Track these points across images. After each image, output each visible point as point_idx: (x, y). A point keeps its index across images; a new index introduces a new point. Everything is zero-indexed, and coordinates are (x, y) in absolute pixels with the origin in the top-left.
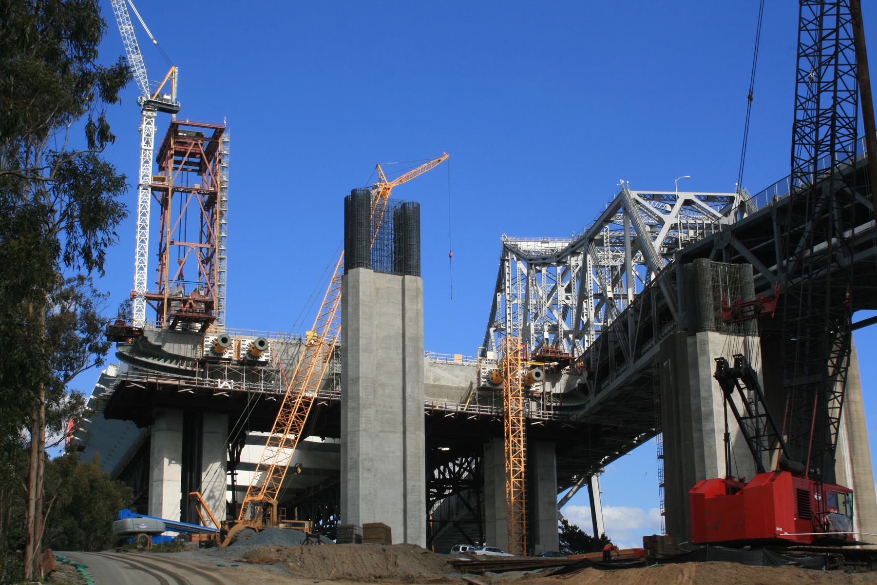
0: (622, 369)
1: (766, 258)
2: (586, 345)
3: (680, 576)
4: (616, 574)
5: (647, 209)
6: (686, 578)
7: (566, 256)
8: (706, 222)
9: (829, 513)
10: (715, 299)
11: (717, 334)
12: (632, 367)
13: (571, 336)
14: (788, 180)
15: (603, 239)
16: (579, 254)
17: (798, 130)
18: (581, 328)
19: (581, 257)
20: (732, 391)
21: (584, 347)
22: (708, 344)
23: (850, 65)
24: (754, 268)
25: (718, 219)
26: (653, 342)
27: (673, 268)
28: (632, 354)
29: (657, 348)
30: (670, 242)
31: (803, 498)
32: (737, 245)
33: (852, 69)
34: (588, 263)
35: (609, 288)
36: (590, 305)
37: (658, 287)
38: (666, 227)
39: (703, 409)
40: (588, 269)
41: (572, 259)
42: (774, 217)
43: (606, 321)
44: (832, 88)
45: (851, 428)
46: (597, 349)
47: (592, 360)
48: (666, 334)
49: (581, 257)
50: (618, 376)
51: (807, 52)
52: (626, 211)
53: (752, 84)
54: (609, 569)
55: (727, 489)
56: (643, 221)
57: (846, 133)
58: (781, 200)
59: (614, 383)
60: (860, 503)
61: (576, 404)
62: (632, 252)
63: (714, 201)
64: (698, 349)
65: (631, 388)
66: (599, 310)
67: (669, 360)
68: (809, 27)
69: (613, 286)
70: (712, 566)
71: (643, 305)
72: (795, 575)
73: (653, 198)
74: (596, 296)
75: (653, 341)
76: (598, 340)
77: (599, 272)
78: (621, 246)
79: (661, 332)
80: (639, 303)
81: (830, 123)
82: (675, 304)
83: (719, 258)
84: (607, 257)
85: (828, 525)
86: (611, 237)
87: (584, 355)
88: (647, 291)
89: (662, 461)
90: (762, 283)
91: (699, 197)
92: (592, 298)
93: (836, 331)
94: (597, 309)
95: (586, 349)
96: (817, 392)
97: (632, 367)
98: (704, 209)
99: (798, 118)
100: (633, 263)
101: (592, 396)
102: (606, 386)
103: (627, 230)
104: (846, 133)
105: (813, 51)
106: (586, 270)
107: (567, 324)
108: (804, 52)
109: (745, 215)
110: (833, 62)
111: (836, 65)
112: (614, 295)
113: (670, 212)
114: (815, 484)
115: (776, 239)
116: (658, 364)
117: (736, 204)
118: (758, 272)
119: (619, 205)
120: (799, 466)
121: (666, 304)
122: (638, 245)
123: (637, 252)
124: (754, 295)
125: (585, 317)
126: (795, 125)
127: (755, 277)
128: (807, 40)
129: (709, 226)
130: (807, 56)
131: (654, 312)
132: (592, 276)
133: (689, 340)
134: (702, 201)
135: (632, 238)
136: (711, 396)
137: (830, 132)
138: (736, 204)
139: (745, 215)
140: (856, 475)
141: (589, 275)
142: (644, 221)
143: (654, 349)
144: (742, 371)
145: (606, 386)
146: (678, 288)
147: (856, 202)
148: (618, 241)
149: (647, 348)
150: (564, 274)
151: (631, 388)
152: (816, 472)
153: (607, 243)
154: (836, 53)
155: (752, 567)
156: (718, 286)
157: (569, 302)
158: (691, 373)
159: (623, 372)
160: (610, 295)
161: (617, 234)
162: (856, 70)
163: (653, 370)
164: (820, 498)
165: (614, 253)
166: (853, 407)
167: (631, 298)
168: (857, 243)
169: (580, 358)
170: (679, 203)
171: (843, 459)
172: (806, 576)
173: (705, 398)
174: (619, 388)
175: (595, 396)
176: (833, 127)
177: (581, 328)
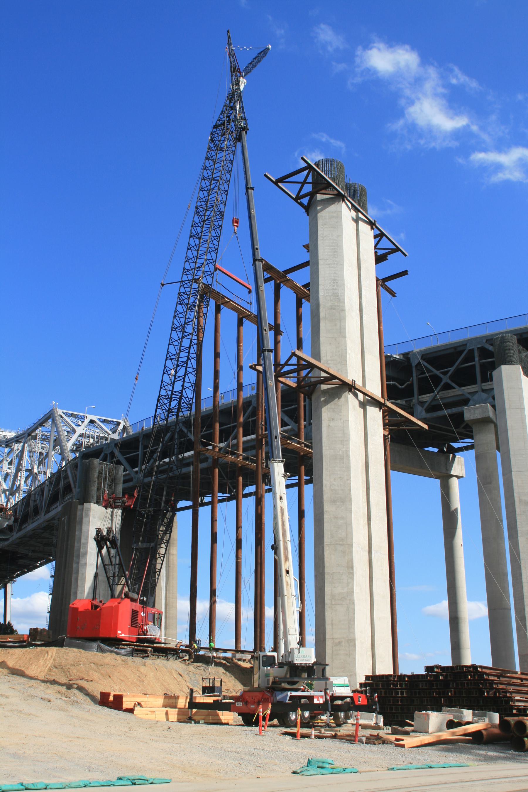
0: (37, 519)
1: (133, 463)
2: (17, 499)
3: (46, 655)
4: (8, 651)
5: (67, 422)
6: (49, 656)
7: (12, 442)
8: (101, 435)
9: (148, 624)
10: (98, 483)
11: (96, 505)
12: (42, 519)
13: (7, 493)
14: (152, 419)
15: (37, 436)
16: (21, 442)
17: (160, 400)
18: (15, 488)
19: (21, 444)
20: (103, 548)
21: (15, 501)
22: (90, 511)
23: (194, 369)
24: (124, 468)
25: (109, 434)
26: (58, 504)
27: (76, 461)
28: (44, 510)
29: (60, 509)
30: (78, 443)
31: (135, 614)
32: (117, 452)
33: (192, 386)
34: (25, 449)
35: (36, 467)
36: (23, 475)
37: (66, 471)
38: (77, 434)
39: (81, 550)
40: (25, 453)
41: (16, 445)
42: (141, 439)
43: (31, 486)
44: (187, 351)
45: (168, 570)
46: (23, 504)
47: (18, 510)
48: (66, 500)
49: (21, 444)
50: (33, 522)
51: (171, 357)
52: (54, 421)
53: (138, 372)
54: (4, 648)
55: (92, 606)
56: (63, 428)
57: (186, 406)
58: (146, 430)
59: (30, 527)
60: (167, 615)
61: (4, 537)
62: (54, 447)
63: (108, 423)
64: (84, 513)
65: (40, 531)
66: (28, 479)
67: (66, 517)
68: (174, 343)
69: (39, 465)
70: (66, 650)
71: (55, 481)
72: (114, 659)
73: (72, 415)
74: (27, 470)
75: (58, 503)
76: (24, 498)
77: (31, 456)
78: (47, 442)
79: (64, 499)
80: (53, 479)
81: (178, 400)
82: (75, 482)
83: (105, 459)
84: (38, 446)
85: (147, 631)
86: (42, 435)
87: (13, 506)
88: (59, 472)
89: (53, 579)
90: (127, 478)
91: (99, 419)
92: (25, 471)
93: (168, 511)
94: (27, 478)
95: (16, 502)
96: (150, 553)
97: (42, 519)
98: (101, 427)
99: (161, 394)
100: (53, 453)
101: (15, 533)
102: (25, 528)
103: (53, 431)
104: (186, 406)
105: (175, 357)
106: (23, 453)
107: (6, 485)
108: (170, 357)
109: (125, 435)
110: (185, 365)
111: (186, 367)
112: (38, 471)
113: (80, 425)
114: (142, 607)
115: (140, 452)
116: (59, 518)
117: (121, 427)
118: (127, 471)
119: (50, 416)
120: (135, 596)
121: (69, 482)
122: (57, 442)
123: (57, 446)
124: (122, 485)
125: (19, 482)
126: (159, 397)
127: (124, 473)
128: (172, 350)
129: (102, 438)
130: (171, 359)
131: (61, 486)
132: (27, 457)
133: (79, 507)
134: (101, 422)
135: (55, 438)
136: (88, 543)
137: (177, 405)
138: (121, 427)
139: (125, 435)
140: (167, 598)
141: (24, 457)
142: (64, 429)
143: (57, 509)
144: (111, 537)
145: (25, 528)
146: (78, 474)
147: (188, 438)
148: (46, 438)
149: (54, 507)
150: (9, 454)
151: (40, 531)
152: (143, 599)
153: (39, 438)
154: (187, 361)
155: (90, 652)
156: (102, 476)
157: (9, 471)
158: (77, 527)
159: (37, 520)
160: (36, 471)
161: (46, 434)
162: (194, 387)
163: (55, 522)
164: (144, 615)
165: (43, 445)
166: (171, 557)
167: (49, 475)
168: (185, 462)
169: (11, 508)
170: (87, 421)
171: (161, 588)
172: (120, 660)
173: (84, 544)
174: (33, 530)
175: (17, 533)
176: (180, 402)
177: (15, 488)
